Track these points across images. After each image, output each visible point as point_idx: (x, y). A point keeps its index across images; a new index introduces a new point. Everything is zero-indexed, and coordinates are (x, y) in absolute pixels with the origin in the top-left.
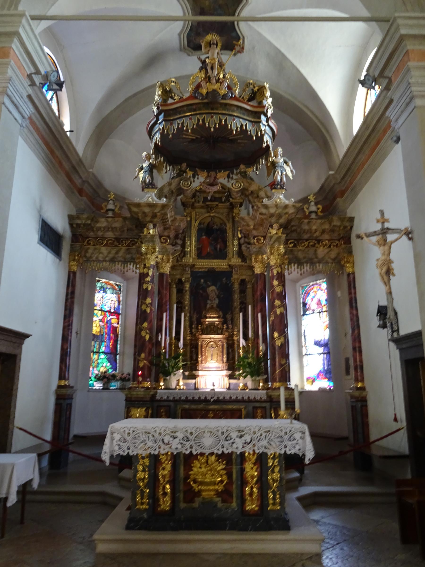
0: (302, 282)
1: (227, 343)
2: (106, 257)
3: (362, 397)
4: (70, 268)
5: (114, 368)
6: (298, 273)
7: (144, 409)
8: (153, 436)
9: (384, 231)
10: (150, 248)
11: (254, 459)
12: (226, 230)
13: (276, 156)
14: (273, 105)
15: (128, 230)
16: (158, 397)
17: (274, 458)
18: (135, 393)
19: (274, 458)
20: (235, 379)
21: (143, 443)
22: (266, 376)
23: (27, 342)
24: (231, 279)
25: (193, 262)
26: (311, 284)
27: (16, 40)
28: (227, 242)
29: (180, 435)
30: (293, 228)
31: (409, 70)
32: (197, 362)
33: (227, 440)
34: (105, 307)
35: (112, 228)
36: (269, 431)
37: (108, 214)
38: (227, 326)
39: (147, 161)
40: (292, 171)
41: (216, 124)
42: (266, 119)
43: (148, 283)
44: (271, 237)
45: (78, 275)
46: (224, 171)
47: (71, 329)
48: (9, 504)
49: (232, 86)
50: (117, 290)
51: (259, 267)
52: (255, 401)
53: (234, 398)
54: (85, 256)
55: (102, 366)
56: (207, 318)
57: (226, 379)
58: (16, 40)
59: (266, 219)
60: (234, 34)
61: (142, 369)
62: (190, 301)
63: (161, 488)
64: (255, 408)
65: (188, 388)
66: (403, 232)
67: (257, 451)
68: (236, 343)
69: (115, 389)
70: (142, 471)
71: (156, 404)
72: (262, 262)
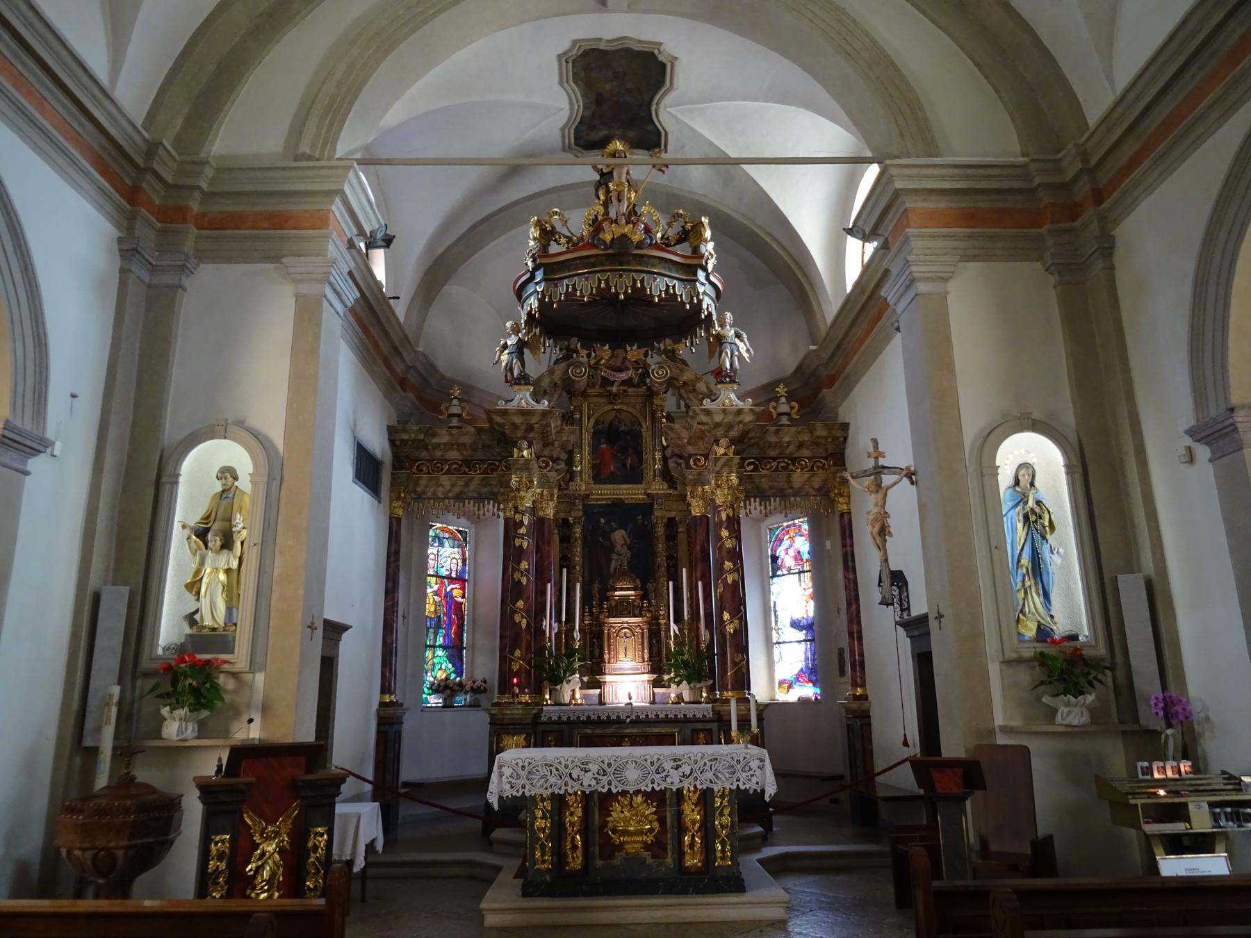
0: (771, 521)
1: (649, 630)
2: (449, 491)
3: (863, 711)
4: (391, 513)
5: (459, 672)
6: (761, 513)
7: (523, 736)
8: (557, 770)
9: (879, 470)
10: (524, 480)
11: (695, 798)
12: (641, 432)
13: (722, 325)
14: (715, 253)
15: (483, 447)
16: (544, 719)
17: (722, 797)
18: (508, 712)
19: (722, 797)
20: (663, 686)
21: (543, 780)
22: (711, 682)
23: (345, 636)
24: (651, 518)
25: (586, 490)
26: (785, 524)
27: (338, 201)
28: (644, 454)
29: (594, 768)
30: (753, 441)
31: (907, 239)
32: (603, 661)
33: (659, 773)
34: (443, 570)
35: (458, 445)
36: (716, 759)
37: (451, 422)
38: (650, 603)
39: (513, 336)
40: (748, 351)
41: (627, 287)
42: (705, 274)
43: (522, 536)
44: (717, 460)
45: (403, 522)
46: (638, 348)
47: (397, 611)
48: (356, 869)
49: (651, 225)
50: (460, 540)
51: (698, 506)
52: (695, 720)
53: (662, 716)
54: (415, 491)
55: (441, 669)
56: (616, 589)
57: (647, 686)
58: (338, 201)
59: (708, 431)
60: (650, 128)
61: (517, 674)
62: (583, 557)
63: (569, 839)
64: (695, 732)
65: (589, 702)
66: (904, 473)
67: (699, 787)
68: (663, 628)
69: (461, 706)
70: (542, 819)
71: (541, 728)
72: (703, 498)
